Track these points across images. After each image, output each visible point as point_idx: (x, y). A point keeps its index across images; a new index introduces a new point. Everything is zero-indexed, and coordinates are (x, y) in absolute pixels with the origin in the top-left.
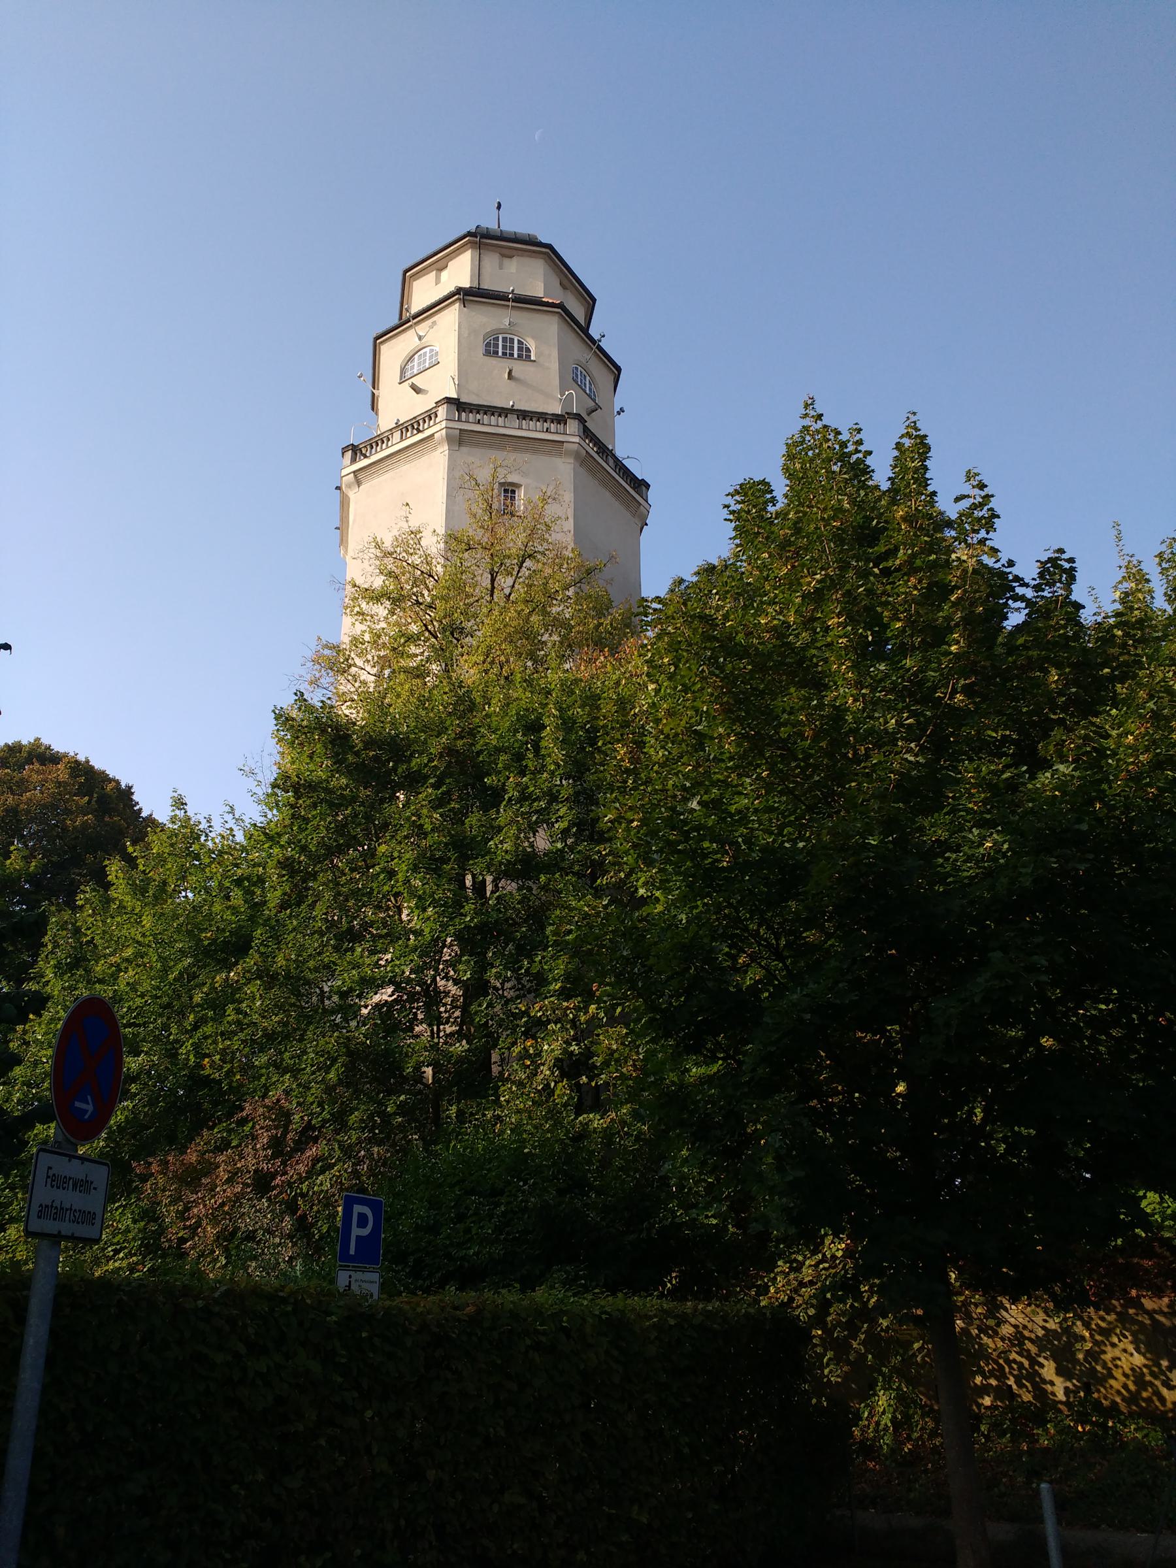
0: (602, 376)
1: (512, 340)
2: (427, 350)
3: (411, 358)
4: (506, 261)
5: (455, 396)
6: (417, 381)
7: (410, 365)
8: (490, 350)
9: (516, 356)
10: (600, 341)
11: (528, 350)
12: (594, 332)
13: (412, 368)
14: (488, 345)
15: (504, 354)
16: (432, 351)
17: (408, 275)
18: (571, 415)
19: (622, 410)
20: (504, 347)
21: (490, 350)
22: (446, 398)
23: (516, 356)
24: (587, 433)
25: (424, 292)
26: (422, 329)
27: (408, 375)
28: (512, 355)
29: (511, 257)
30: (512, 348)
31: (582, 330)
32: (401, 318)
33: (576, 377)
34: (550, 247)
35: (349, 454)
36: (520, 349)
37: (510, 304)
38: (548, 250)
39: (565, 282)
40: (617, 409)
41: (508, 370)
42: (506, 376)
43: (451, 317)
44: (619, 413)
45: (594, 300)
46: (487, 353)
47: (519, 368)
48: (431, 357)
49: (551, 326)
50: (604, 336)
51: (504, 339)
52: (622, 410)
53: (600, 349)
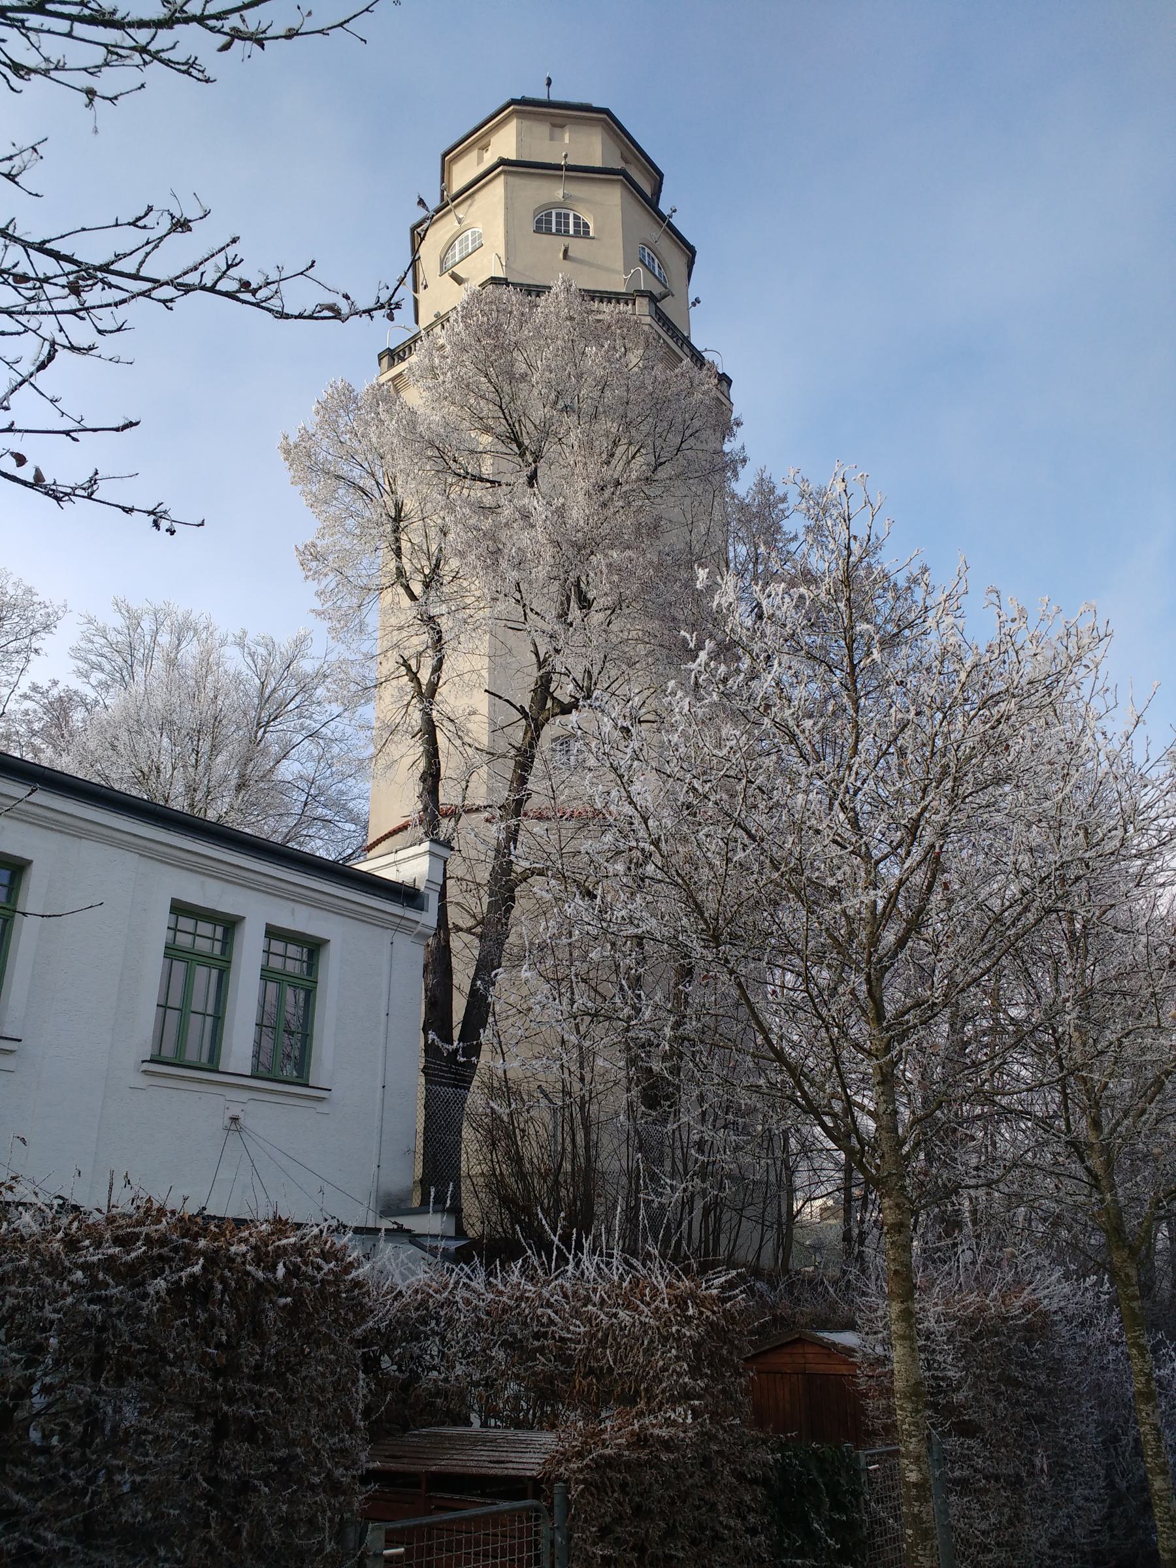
0: (676, 261)
1: (567, 216)
2: (469, 232)
3: (450, 246)
4: (557, 130)
5: (502, 275)
6: (459, 270)
7: (451, 253)
8: (542, 226)
9: (571, 232)
10: (671, 217)
11: (586, 226)
12: (664, 206)
13: (454, 256)
14: (539, 221)
15: (558, 231)
16: (473, 233)
17: (449, 158)
18: (642, 294)
19: (697, 301)
20: (558, 224)
21: (542, 226)
22: (493, 278)
23: (571, 232)
24: (662, 318)
25: (463, 173)
26: (460, 212)
27: (449, 264)
28: (568, 231)
29: (562, 126)
30: (567, 224)
31: (650, 202)
32: (442, 199)
33: (646, 258)
34: (606, 112)
35: (385, 361)
36: (576, 225)
37: (563, 173)
38: (604, 116)
39: (627, 154)
40: (692, 299)
41: (563, 248)
42: (561, 256)
43: (497, 190)
44: (694, 304)
45: (661, 175)
46: (538, 230)
47: (578, 247)
48: (474, 241)
49: (612, 197)
50: (675, 211)
51: (558, 215)
52: (697, 301)
53: (671, 227)
